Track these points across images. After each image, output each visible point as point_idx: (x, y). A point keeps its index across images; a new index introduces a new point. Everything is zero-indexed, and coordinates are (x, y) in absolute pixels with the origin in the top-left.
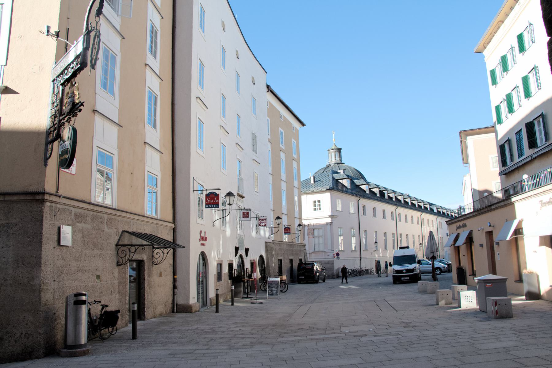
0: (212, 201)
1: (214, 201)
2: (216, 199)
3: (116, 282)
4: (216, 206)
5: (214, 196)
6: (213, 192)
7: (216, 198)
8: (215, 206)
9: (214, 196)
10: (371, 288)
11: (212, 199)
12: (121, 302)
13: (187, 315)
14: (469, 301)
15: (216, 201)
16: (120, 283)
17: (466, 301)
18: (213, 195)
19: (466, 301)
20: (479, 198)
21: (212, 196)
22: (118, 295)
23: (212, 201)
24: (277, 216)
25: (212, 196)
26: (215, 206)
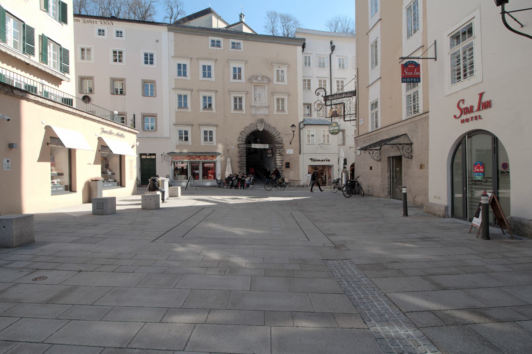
0: (478, 170)
1: (413, 73)
2: (417, 71)
3: (380, 171)
4: (416, 80)
5: (413, 66)
6: (413, 62)
7: (416, 69)
8: (415, 80)
9: (413, 66)
10: (7, 92)
11: (412, 70)
12: (382, 182)
13: (404, 163)
14: (98, 206)
15: (416, 73)
16: (382, 171)
17: (98, 203)
18: (413, 65)
19: (103, 204)
20: (422, 44)
21: (411, 66)
22: (380, 178)
23: (478, 170)
24: (292, 124)
25: (411, 66)
26: (415, 80)
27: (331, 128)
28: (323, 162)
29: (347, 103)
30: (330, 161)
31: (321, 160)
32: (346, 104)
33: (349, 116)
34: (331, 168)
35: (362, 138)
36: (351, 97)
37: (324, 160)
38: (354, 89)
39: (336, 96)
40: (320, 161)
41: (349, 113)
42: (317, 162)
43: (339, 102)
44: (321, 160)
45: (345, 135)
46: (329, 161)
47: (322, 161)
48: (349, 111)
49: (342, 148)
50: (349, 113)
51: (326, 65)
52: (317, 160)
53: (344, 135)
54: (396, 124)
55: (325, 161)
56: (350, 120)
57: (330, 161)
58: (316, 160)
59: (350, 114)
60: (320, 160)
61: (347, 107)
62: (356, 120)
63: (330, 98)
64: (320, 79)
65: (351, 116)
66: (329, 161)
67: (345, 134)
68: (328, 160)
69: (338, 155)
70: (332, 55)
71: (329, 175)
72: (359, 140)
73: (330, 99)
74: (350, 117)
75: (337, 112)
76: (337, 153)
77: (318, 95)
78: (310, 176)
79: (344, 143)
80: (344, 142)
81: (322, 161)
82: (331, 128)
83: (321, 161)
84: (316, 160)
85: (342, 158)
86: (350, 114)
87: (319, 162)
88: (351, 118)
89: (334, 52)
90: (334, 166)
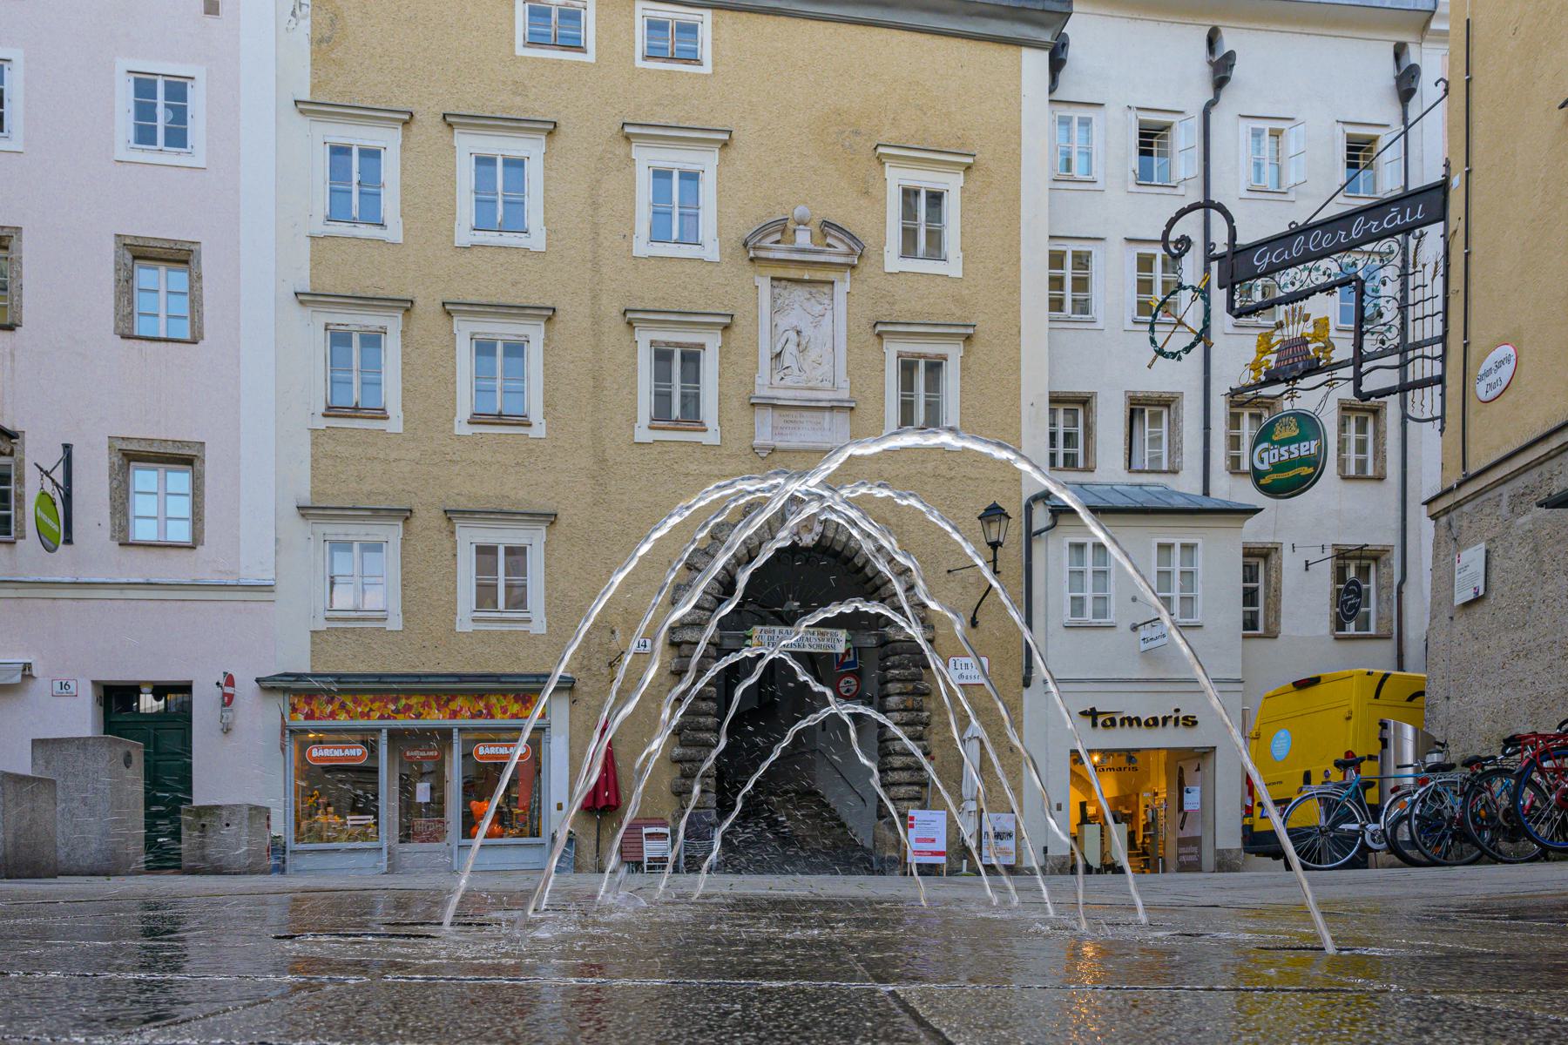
27: (1265, 455)
30: (1195, 723)
37: (1165, 720)
39: (1306, 243)
43: (1323, 279)
46: (1191, 722)
55: (1171, 723)
57: (1195, 723)
62: (1440, 380)
66: (1191, 722)
68: (1185, 718)
70: (1214, 115)
73: (1262, 266)
82: (1265, 455)
90: (1218, 752)
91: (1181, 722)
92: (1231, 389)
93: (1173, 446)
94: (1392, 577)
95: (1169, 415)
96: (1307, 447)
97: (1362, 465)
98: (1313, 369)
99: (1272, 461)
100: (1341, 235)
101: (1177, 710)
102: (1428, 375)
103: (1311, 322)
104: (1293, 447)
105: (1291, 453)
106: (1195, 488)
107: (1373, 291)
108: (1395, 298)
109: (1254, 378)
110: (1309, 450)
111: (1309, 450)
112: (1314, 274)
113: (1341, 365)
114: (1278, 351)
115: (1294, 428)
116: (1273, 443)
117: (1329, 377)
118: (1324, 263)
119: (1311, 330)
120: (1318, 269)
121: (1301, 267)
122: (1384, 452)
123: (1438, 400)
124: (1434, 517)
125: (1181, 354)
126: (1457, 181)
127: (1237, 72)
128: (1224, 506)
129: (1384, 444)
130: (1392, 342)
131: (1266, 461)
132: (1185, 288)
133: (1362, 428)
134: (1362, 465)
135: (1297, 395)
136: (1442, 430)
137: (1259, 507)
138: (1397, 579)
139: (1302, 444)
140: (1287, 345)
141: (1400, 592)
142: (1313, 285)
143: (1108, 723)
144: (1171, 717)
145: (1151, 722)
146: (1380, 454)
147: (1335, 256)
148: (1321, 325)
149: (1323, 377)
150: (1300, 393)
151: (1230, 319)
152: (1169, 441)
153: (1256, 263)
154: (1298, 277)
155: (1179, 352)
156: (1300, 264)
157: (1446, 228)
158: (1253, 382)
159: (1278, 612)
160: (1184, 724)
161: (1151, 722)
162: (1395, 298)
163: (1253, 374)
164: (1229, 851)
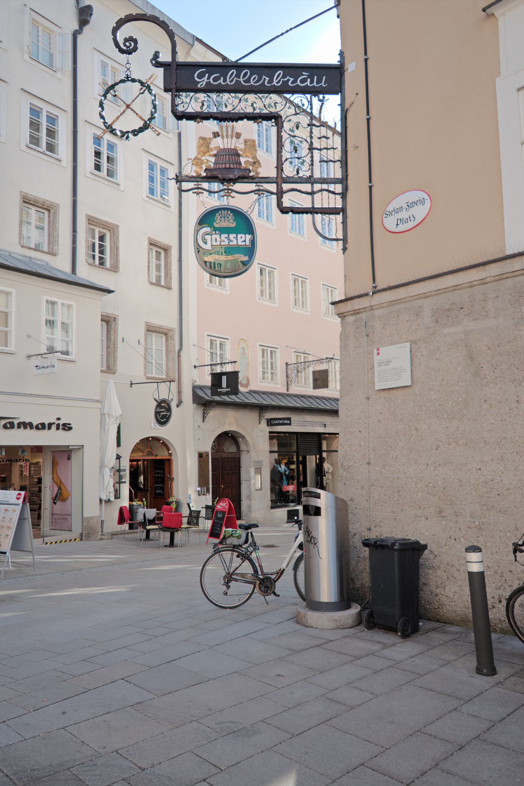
27: (208, 237)
28: (45, 432)
29: (295, 119)
30: (70, 429)
31: (34, 425)
32: (292, 125)
33: (307, 187)
34: (69, 459)
35: (426, 296)
36: (315, 92)
37: (50, 425)
38: (334, 60)
39: (238, 76)
40: (34, 431)
41: (308, 174)
42: (22, 430)
43: (250, 110)
44: (34, 425)
45: (116, 339)
46: (67, 427)
47: (42, 427)
48: (308, 159)
49: (111, 379)
50: (305, 173)
51: (58, 62)
52: (19, 425)
53: (112, 337)
54: (450, 277)
55: (54, 427)
56: (312, 211)
57: (70, 429)
58: (16, 422)
59: (310, 180)
60: (30, 425)
61: (296, 141)
62: (343, 211)
63: (201, 76)
64: (39, 104)
65: (317, 187)
66: (67, 427)
67: (116, 332)
68: (64, 425)
69: (99, 405)
70: (80, 38)
71: (60, 489)
72: (377, 313)
73: (203, 83)
74: (312, 193)
75: (242, 160)
76: (98, 398)
77: (129, 52)
78: (14, 500)
79: (112, 367)
80: (111, 362)
81: (42, 427)
82: (208, 237)
83: (37, 428)
84: (16, 422)
85: (112, 420)
86: (310, 180)
87: (28, 431)
88: (317, 196)
89: (86, 29)
90: (85, 448)
91: (61, 427)
92: (339, 105)
93: (51, 237)
94: (174, 346)
95: (49, 217)
96: (243, 239)
97: (158, 278)
98: (245, 178)
99: (214, 243)
100: (265, 79)
101: (59, 419)
102: (332, 206)
103: (241, 140)
104: (232, 236)
105: (230, 240)
106: (67, 268)
107: (290, 130)
108: (306, 141)
109: (196, 172)
110: (245, 241)
111: (245, 241)
112: (242, 104)
113: (267, 180)
114: (215, 155)
115: (231, 221)
116: (215, 229)
117: (257, 188)
118: (251, 97)
119: (242, 146)
120: (246, 101)
121: (233, 95)
122: (171, 274)
123: (340, 226)
124: (342, 316)
125: (130, 135)
126: (351, 67)
127: (93, 19)
128: (90, 285)
129: (170, 270)
130: (305, 173)
131: (209, 242)
132: (133, 80)
133: (158, 258)
134: (158, 278)
135: (232, 195)
136: (345, 249)
137: (112, 289)
138: (177, 348)
139: (239, 236)
140: (220, 154)
141: (179, 356)
142: (242, 112)
143: (8, 426)
144: (54, 423)
145: (40, 427)
146: (168, 274)
147: (260, 95)
148: (251, 145)
149: (252, 187)
150: (233, 194)
151: (171, 119)
152: (49, 234)
153: (196, 79)
154: (230, 101)
155: (128, 132)
156: (233, 92)
157: (343, 99)
158: (194, 174)
159: (115, 357)
160: (63, 429)
161: (40, 427)
162: (306, 141)
163: (194, 168)
164: (92, 518)
